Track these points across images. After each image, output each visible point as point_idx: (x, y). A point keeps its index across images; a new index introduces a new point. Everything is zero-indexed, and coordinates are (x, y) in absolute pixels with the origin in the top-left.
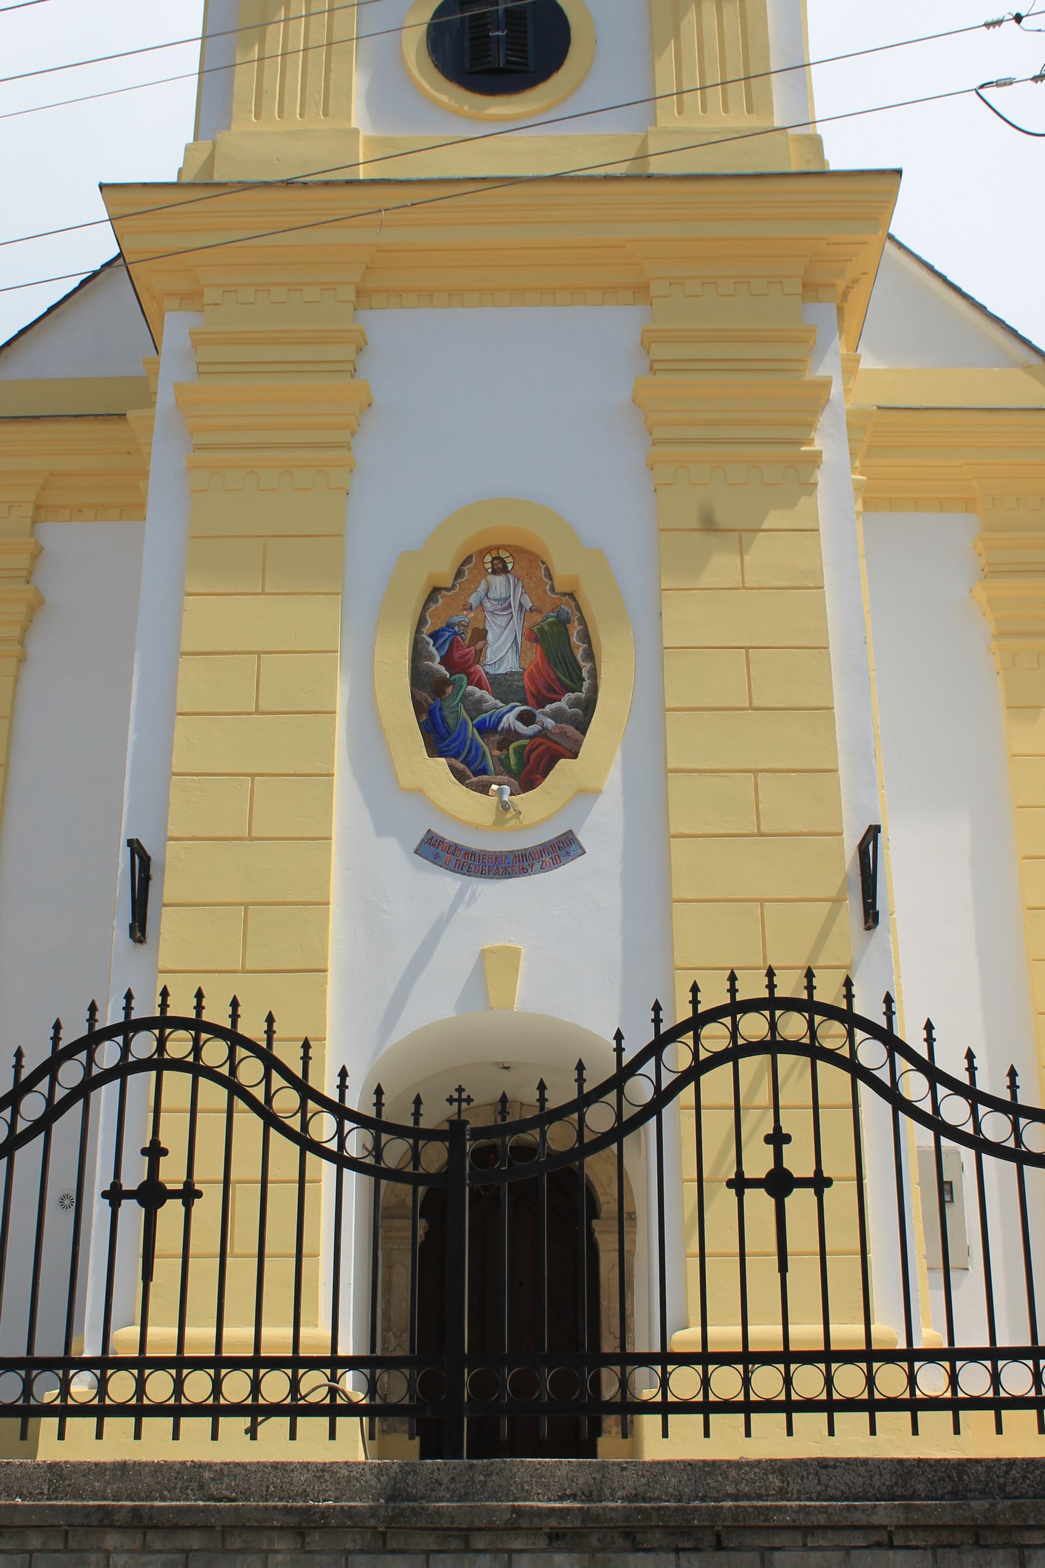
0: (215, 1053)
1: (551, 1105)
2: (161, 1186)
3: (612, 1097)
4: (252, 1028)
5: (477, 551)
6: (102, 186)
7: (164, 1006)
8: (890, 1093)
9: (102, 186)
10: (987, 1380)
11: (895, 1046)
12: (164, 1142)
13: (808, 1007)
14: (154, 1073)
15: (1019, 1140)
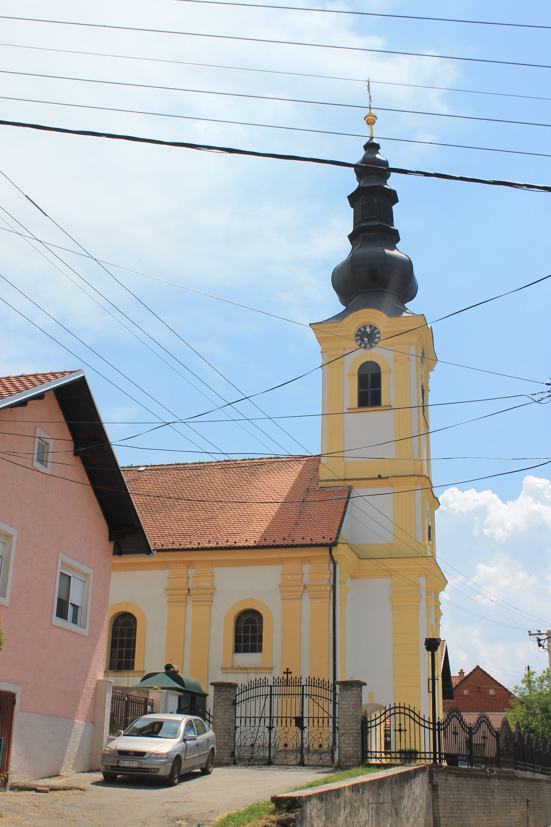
0: (402, 710)
2: (401, 729)
4: (412, 709)
8: (414, 720)
10: (421, 756)
11: (415, 714)
12: (401, 724)
13: (404, 708)
15: (429, 726)
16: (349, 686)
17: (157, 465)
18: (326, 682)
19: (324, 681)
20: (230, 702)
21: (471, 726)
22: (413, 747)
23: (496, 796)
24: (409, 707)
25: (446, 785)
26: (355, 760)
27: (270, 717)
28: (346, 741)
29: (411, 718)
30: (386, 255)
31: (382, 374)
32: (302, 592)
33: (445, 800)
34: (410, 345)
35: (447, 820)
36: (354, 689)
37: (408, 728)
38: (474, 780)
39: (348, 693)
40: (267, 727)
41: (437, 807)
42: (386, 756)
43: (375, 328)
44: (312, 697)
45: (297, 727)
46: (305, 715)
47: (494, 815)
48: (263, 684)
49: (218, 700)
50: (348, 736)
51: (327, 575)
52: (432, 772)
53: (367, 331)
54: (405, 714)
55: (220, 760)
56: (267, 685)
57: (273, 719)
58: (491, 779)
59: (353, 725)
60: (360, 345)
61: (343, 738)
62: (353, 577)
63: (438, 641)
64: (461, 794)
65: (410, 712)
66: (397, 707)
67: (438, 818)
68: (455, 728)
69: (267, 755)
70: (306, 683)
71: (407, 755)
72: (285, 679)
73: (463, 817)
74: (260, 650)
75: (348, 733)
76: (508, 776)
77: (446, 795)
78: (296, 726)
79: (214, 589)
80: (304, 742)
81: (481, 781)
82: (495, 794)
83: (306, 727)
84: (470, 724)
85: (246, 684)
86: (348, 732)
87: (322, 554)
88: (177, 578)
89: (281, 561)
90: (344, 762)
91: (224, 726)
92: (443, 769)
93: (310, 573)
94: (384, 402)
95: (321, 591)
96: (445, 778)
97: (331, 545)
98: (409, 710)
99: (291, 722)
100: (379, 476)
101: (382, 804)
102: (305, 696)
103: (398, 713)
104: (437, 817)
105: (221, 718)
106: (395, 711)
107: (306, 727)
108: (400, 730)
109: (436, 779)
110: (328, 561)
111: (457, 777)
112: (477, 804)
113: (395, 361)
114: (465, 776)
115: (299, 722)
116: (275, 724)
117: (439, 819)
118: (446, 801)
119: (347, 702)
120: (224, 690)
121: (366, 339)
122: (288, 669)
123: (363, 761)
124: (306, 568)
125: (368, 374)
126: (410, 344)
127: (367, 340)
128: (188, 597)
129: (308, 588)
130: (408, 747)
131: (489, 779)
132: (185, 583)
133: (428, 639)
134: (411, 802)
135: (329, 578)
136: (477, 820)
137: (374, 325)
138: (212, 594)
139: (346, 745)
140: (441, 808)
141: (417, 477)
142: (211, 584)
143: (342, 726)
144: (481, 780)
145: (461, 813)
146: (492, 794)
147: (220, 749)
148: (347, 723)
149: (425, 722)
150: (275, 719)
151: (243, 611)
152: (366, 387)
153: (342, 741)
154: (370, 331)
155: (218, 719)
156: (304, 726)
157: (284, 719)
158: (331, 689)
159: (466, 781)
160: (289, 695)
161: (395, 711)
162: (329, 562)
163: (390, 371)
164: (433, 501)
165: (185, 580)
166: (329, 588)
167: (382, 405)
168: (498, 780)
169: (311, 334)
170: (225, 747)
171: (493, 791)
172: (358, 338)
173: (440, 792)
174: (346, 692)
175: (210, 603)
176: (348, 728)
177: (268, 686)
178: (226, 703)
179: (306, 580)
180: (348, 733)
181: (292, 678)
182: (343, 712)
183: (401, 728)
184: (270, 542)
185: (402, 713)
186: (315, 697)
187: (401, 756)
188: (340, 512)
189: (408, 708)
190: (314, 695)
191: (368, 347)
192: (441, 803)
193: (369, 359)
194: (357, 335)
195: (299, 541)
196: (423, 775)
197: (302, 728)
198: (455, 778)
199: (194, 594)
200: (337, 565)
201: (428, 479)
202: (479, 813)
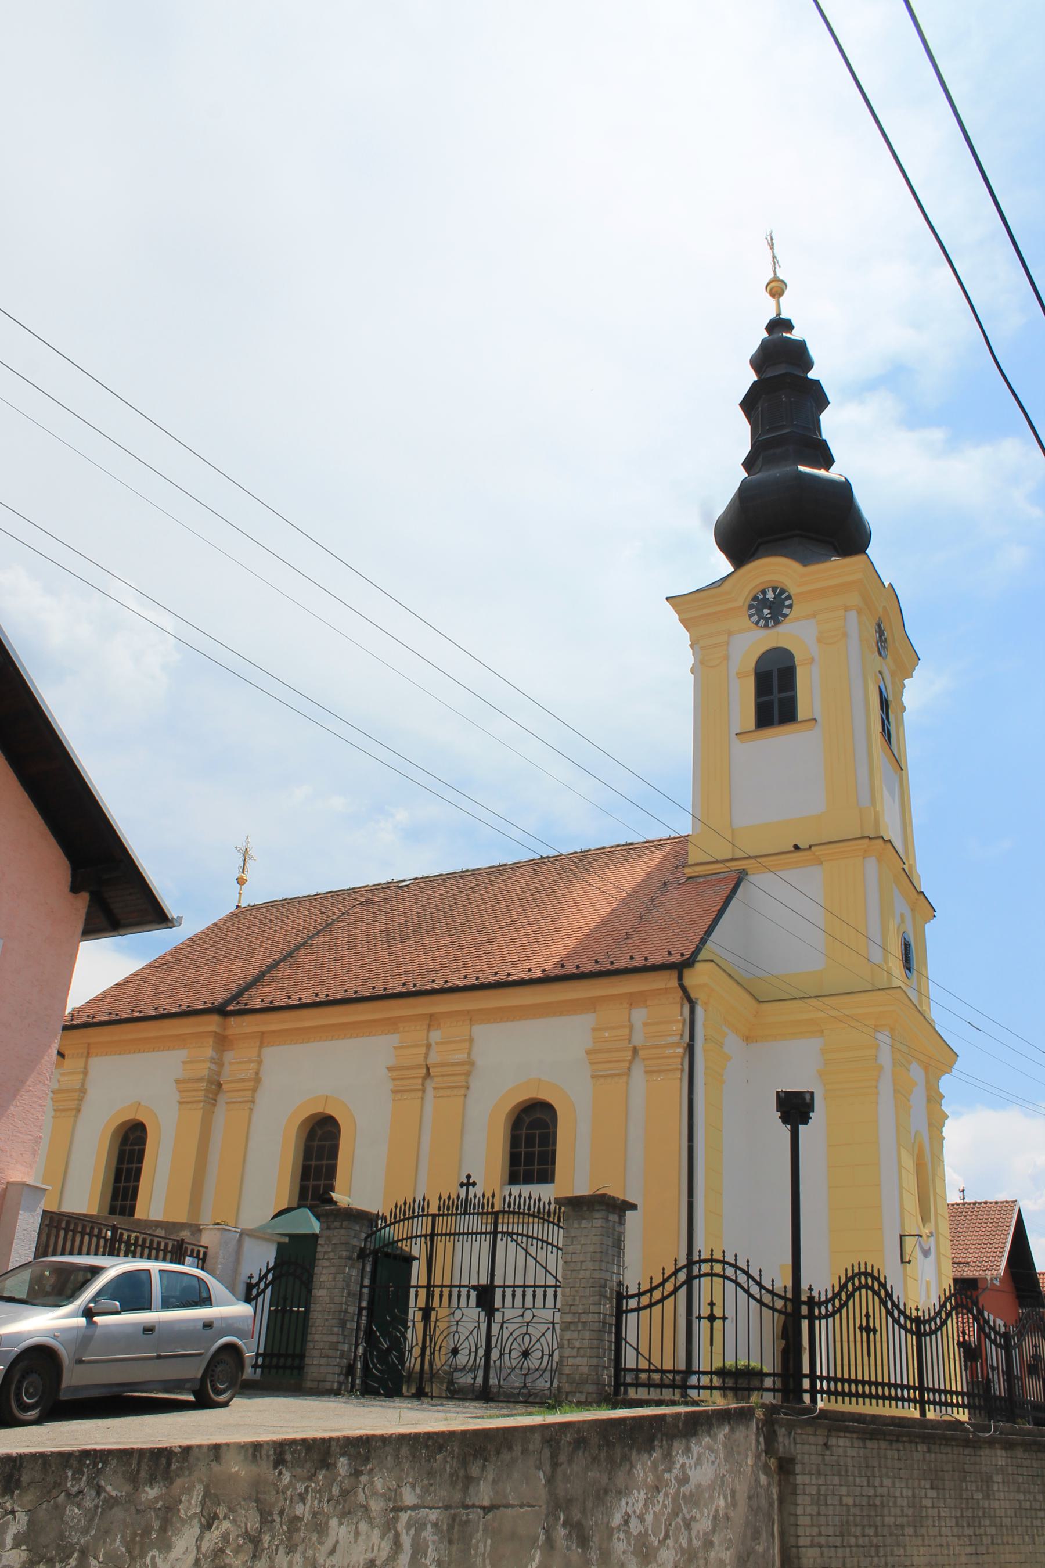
0: (730, 1272)
3: (661, 1288)
4: (741, 1263)
6: (667, 599)
7: (712, 1255)
8: (747, 1291)
9: (667, 599)
11: (749, 1276)
12: (714, 1302)
14: (698, 1280)
16: (585, 1209)
17: (431, 875)
18: (544, 1203)
19: (540, 1200)
20: (347, 1251)
22: (755, 1364)
23: (998, 1491)
24: (736, 1260)
25: (824, 1460)
26: (591, 1388)
27: (429, 1286)
28: (575, 1342)
29: (738, 1288)
30: (801, 472)
31: (797, 668)
32: (631, 1062)
33: (819, 1499)
34: (846, 611)
35: (826, 1554)
36: (597, 1215)
37: (730, 1313)
38: (925, 1449)
39: (583, 1226)
40: (420, 1309)
41: (792, 1519)
42: (649, 1377)
43: (783, 591)
44: (515, 1237)
45: (480, 1309)
46: (498, 1281)
47: (992, 1540)
48: (418, 1213)
49: (326, 1246)
50: (580, 1329)
51: (677, 1028)
52: (773, 1425)
53: (767, 597)
54: (724, 1277)
56: (425, 1213)
57: (433, 1291)
58: (980, 1448)
59: (590, 1302)
60: (757, 623)
61: (568, 1335)
62: (748, 1039)
63: (808, 1097)
64: (877, 1484)
65: (738, 1272)
67: (794, 1550)
68: (867, 1316)
69: (480, 1380)
70: (504, 1208)
71: (726, 1380)
72: (462, 1199)
73: (885, 1546)
75: (579, 1322)
76: (1035, 1443)
77: (823, 1488)
78: (478, 1306)
79: (472, 1064)
80: (493, 1345)
81: (947, 1454)
82: (995, 1488)
83: (498, 1310)
84: (917, 1309)
86: (579, 1319)
87: (666, 985)
89: (591, 1005)
91: (332, 1305)
92: (813, 1418)
93: (645, 1024)
94: (802, 713)
95: (664, 1058)
96: (821, 1440)
97: (681, 967)
98: (735, 1266)
100: (796, 847)
101: (487, 1510)
102: (499, 1236)
103: (705, 1275)
104: (793, 1546)
105: (328, 1286)
107: (498, 1310)
108: (712, 1318)
109: (784, 1443)
110: (678, 999)
111: (864, 1440)
112: (930, 1512)
113: (819, 640)
114: (895, 1438)
115: (485, 1296)
116: (436, 1303)
117: (798, 1552)
118: (822, 1503)
119: (579, 1247)
120: (337, 1224)
121: (766, 611)
122: (469, 1177)
123: (617, 1392)
124: (639, 1015)
125: (772, 670)
126: (847, 609)
127: (769, 611)
128: (428, 1082)
129: (641, 1052)
130: (742, 1363)
131: (974, 1447)
132: (423, 1055)
133: (783, 1095)
134: (665, 1506)
135: (680, 1032)
136: (936, 1555)
137: (780, 585)
138: (468, 1074)
139: (574, 1352)
140: (804, 1521)
141: (866, 841)
142: (466, 1056)
143: (567, 1305)
144: (944, 1449)
145: (876, 1535)
146: (984, 1487)
147: (321, 1357)
148: (577, 1298)
149: (775, 1298)
150: (437, 1291)
151: (529, 1104)
152: (770, 692)
153: (566, 1342)
154: (773, 596)
155: (323, 1288)
156: (496, 1306)
157: (455, 1290)
158: (554, 1219)
159: (898, 1450)
162: (682, 1001)
163: (812, 660)
164: (916, 899)
165: (423, 1050)
166: (680, 1050)
167: (799, 719)
168: (1003, 1452)
169: (671, 616)
170: (331, 1353)
171: (988, 1480)
172: (753, 611)
173: (799, 1479)
174: (580, 1224)
175: (463, 1091)
176: (580, 1312)
177: (428, 1215)
178: (341, 1253)
179: (638, 1040)
180: (579, 1322)
181: (475, 1197)
182: (571, 1271)
183: (714, 1313)
184: (570, 969)
186: (520, 1237)
187: (724, 1382)
188: (713, 912)
189: (734, 1262)
191: (771, 623)
192: (804, 1508)
193: (774, 645)
194: (751, 607)
195: (622, 963)
196: (732, 1430)
198: (856, 1443)
199: (436, 1076)
200: (696, 1005)
201: (889, 844)
202: (941, 1535)
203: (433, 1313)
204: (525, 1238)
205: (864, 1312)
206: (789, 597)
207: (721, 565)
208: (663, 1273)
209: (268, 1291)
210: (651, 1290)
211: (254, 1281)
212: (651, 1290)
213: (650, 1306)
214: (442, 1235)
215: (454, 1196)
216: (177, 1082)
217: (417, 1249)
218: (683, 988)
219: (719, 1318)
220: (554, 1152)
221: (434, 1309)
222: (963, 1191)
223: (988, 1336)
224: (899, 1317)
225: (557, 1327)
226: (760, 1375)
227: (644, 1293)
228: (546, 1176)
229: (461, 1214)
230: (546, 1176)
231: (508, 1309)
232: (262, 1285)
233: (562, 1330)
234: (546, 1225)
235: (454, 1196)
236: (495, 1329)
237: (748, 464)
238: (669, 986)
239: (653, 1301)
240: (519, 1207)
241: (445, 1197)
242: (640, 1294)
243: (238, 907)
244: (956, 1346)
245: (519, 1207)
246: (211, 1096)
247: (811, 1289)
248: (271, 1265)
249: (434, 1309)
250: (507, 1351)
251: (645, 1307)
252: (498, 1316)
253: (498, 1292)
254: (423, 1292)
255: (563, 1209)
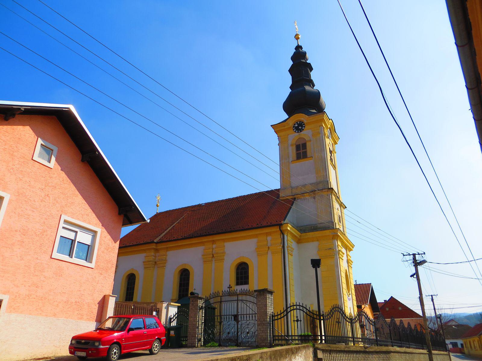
0: (301, 308)
1: (278, 314)
5: (297, 244)
6: (271, 126)
9: (271, 126)
11: (307, 309)
13: (299, 306)
21: (352, 317)
32: (268, 251)
37: (302, 319)
40: (219, 322)
55: (192, 344)
60: (295, 132)
61: (260, 327)
65: (304, 308)
66: (295, 305)
68: (338, 318)
74: (248, 284)
83: (240, 321)
85: (208, 296)
88: (208, 249)
90: (260, 343)
98: (302, 306)
99: (231, 318)
103: (295, 309)
106: (293, 308)
115: (236, 317)
124: (269, 238)
128: (213, 258)
150: (223, 317)
153: (259, 329)
156: (239, 320)
160: (230, 301)
161: (293, 308)
181: (232, 291)
185: (298, 309)
187: (301, 338)
190: (244, 300)
197: (238, 322)
203: (222, 323)
204: (249, 302)
205: (337, 318)
206: (304, 124)
207: (286, 116)
208: (284, 309)
209: (176, 319)
210: (281, 314)
211: (172, 317)
212: (281, 314)
213: (281, 318)
214: (223, 301)
215: (226, 291)
216: (144, 262)
217: (217, 306)
218: (281, 230)
219: (295, 321)
220: (248, 276)
221: (222, 322)
222: (356, 281)
223: (346, 320)
224: (346, 318)
225: (256, 325)
226: (308, 336)
227: (279, 315)
228: (246, 283)
229: (228, 296)
230: (246, 283)
231: (243, 322)
232: (174, 318)
233: (257, 326)
234: (246, 296)
235: (226, 291)
236: (239, 326)
237: (291, 87)
238: (277, 230)
239: (281, 317)
240: (241, 293)
241: (224, 291)
242: (278, 315)
243: (157, 213)
244: (341, 322)
245: (241, 293)
246: (153, 265)
247: (323, 312)
248: (176, 312)
249: (222, 322)
250: (243, 332)
251: (279, 319)
252: (240, 323)
253: (240, 316)
254: (219, 317)
255: (256, 293)
